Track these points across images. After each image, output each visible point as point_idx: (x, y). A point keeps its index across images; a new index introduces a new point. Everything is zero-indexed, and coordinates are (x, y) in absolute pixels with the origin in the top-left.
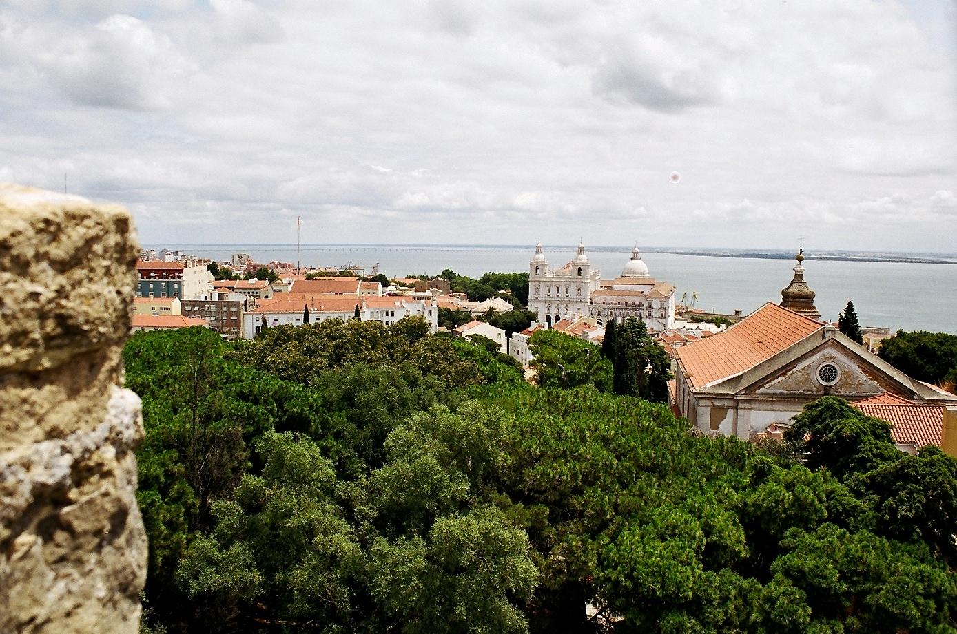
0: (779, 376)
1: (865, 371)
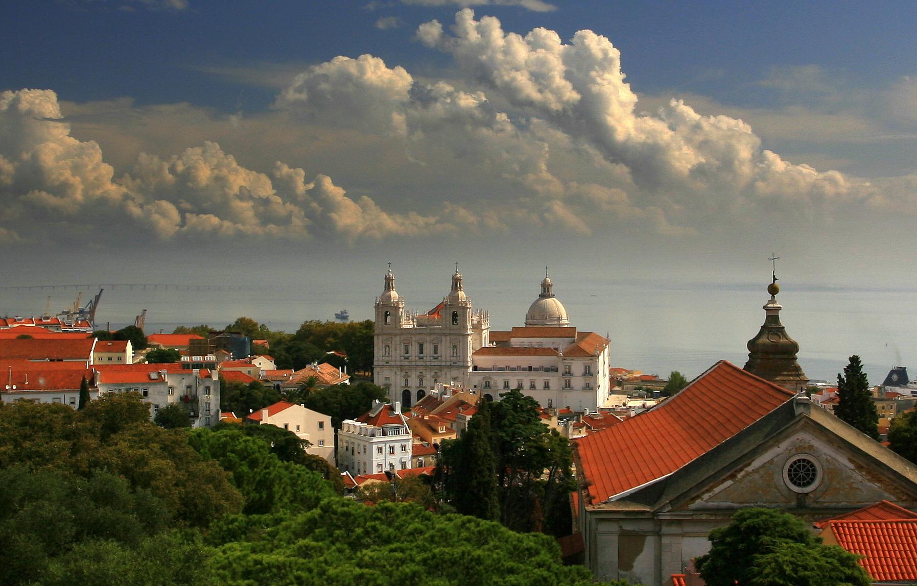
0: (724, 480)
1: (859, 467)
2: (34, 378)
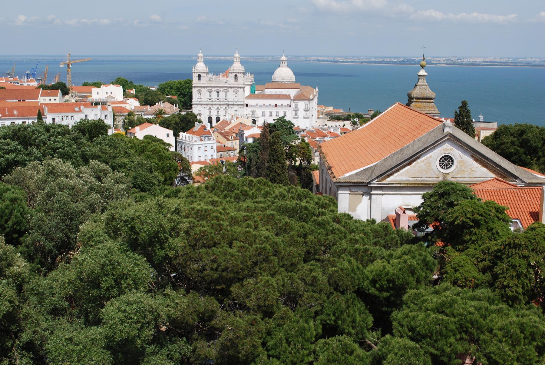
2: (11, 110)
